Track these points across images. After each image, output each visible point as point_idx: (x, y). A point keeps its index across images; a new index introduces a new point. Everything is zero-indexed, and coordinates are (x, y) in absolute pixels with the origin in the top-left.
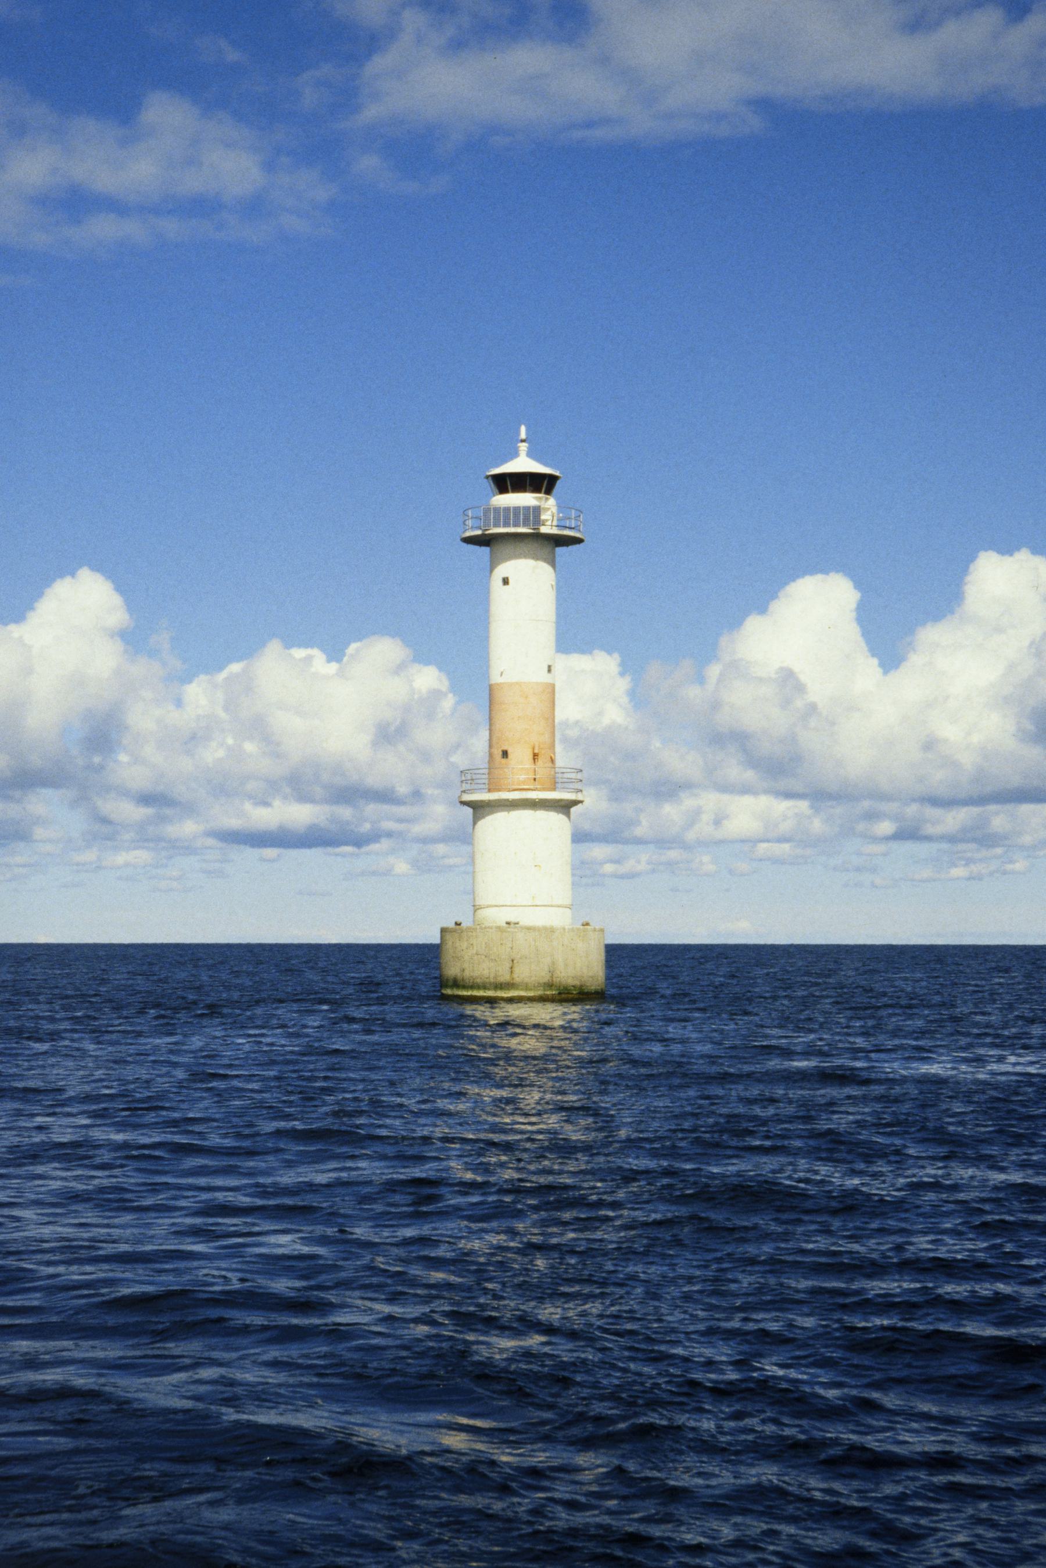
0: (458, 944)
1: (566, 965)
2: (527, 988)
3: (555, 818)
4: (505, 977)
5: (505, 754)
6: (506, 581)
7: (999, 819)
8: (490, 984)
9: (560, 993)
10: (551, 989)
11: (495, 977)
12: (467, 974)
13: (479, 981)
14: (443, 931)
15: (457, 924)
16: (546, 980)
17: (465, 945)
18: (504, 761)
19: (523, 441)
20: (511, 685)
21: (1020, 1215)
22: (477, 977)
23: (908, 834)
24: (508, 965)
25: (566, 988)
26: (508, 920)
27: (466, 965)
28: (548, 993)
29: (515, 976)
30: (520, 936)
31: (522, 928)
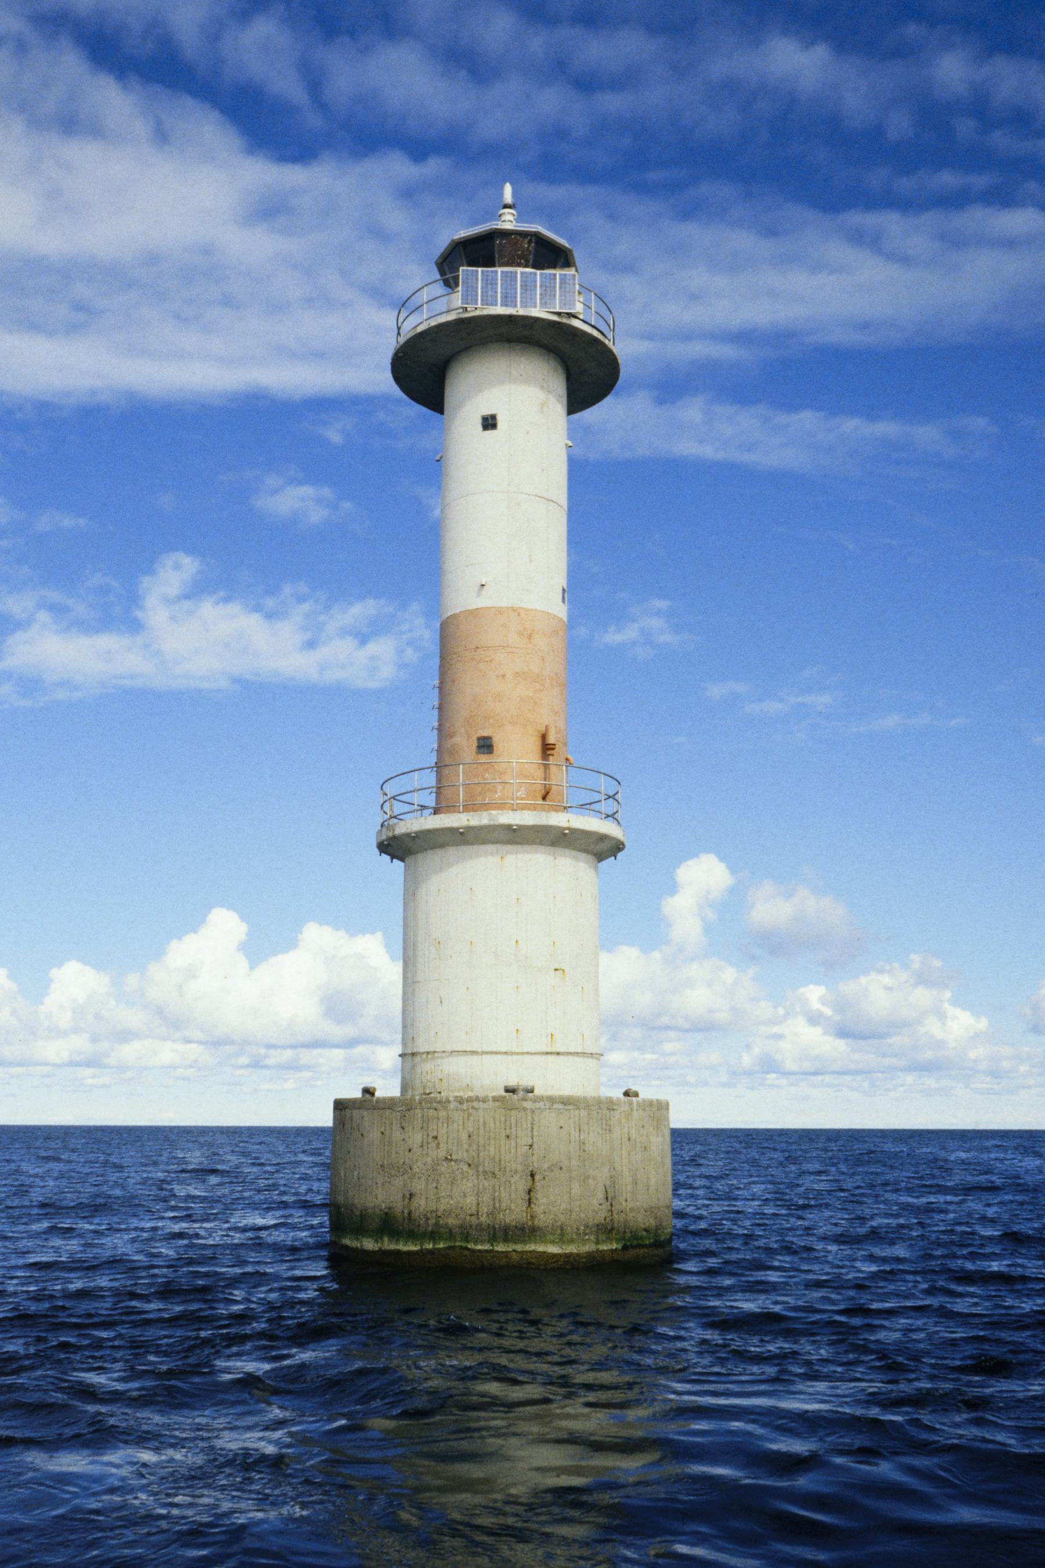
0: (397, 1135)
1: (635, 1183)
2: (561, 1235)
3: (571, 870)
4: (514, 1213)
5: (486, 745)
6: (489, 423)
7: (306, 1056)
8: (480, 1227)
9: (625, 1248)
10: (609, 1239)
11: (491, 1214)
12: (421, 1205)
13: (452, 1221)
14: (340, 1106)
15: (627, 1094)
16: (601, 1216)
17: (416, 1138)
18: (484, 758)
19: (506, 206)
20: (500, 611)
21: (660, 1348)
22: (448, 1213)
23: (256, 1064)
24: (521, 1185)
25: (635, 1236)
26: (512, 1083)
27: (418, 1186)
28: (604, 1247)
29: (538, 1209)
30: (549, 1120)
31: (540, 1099)
